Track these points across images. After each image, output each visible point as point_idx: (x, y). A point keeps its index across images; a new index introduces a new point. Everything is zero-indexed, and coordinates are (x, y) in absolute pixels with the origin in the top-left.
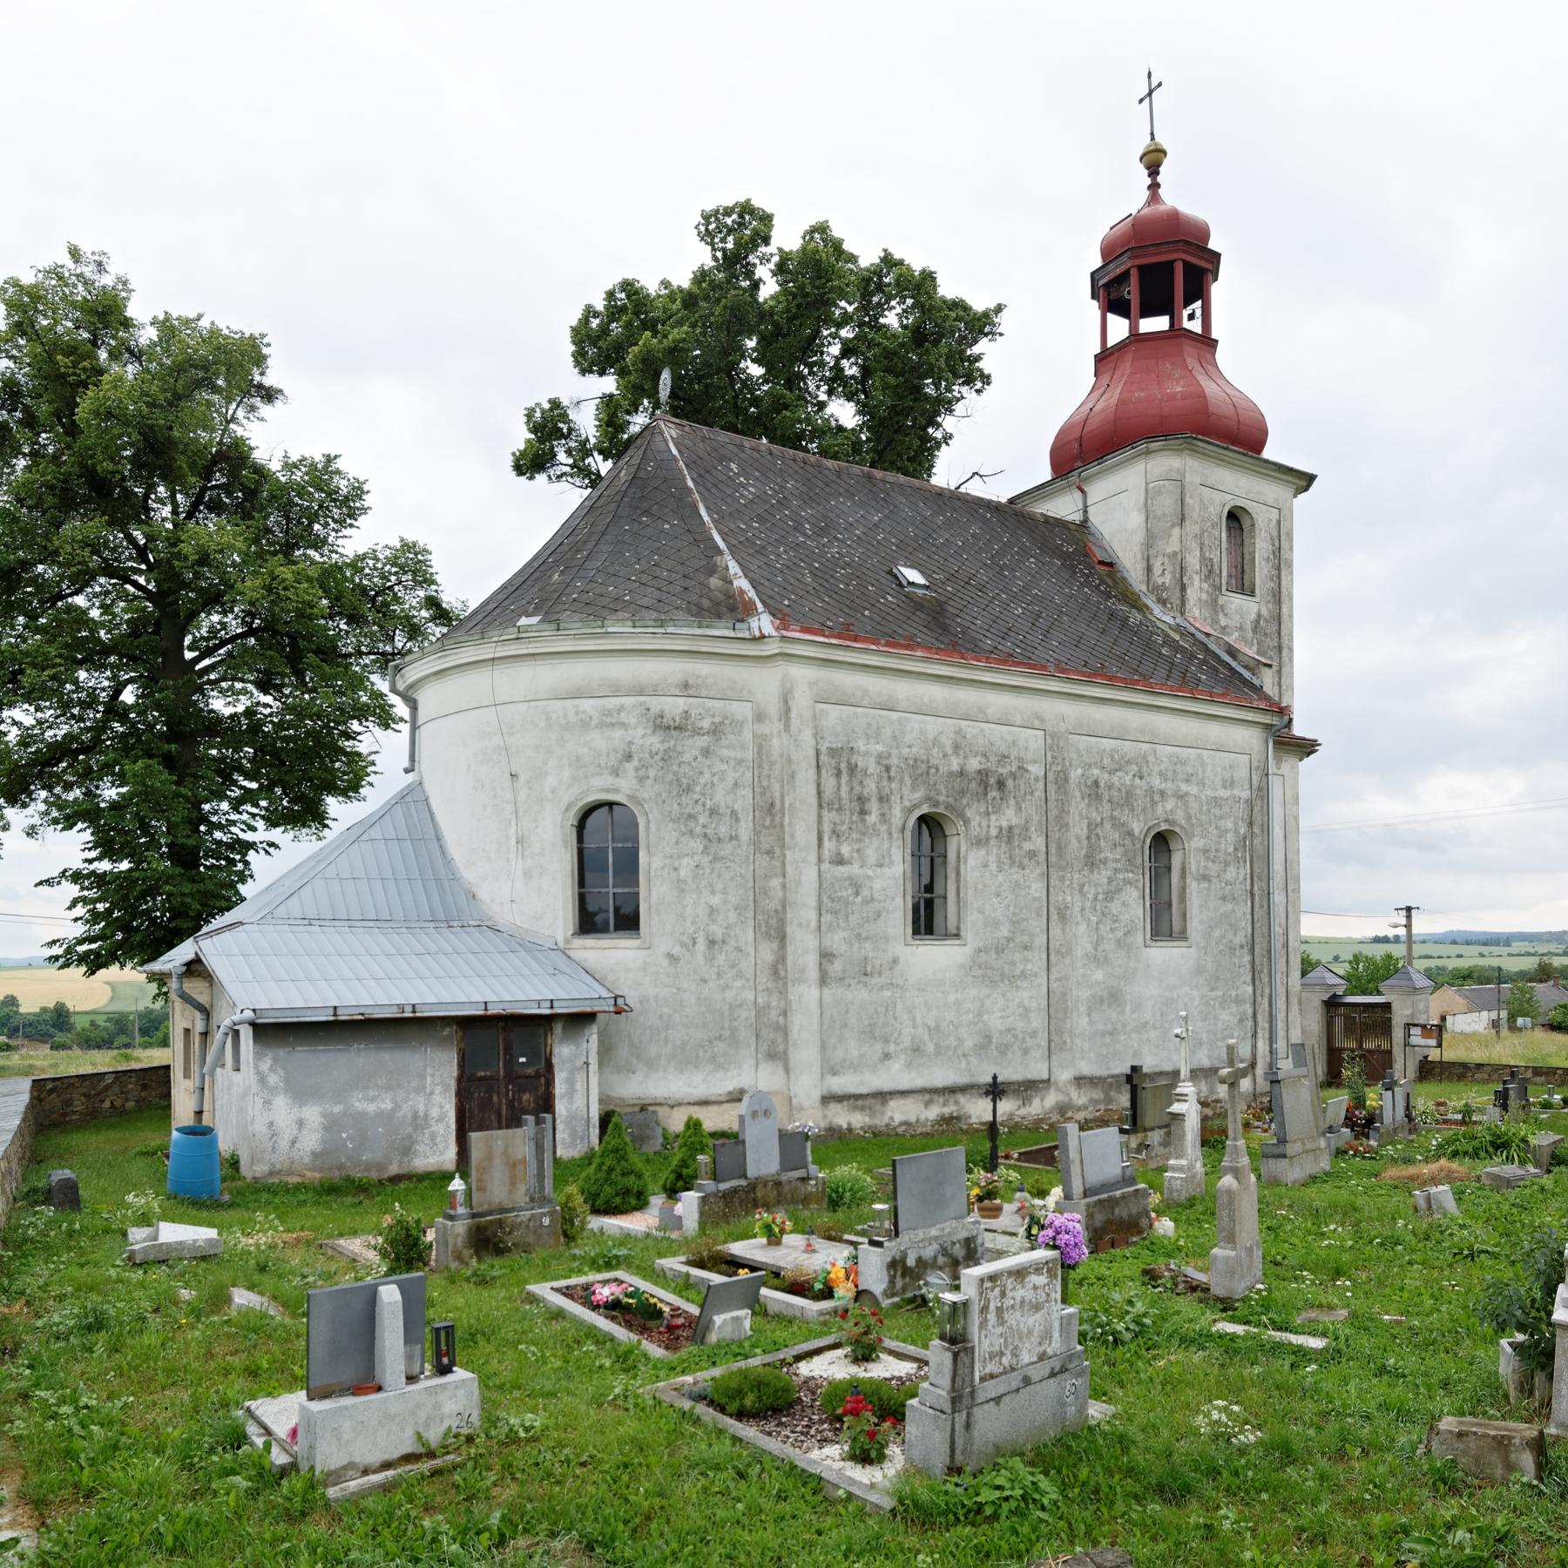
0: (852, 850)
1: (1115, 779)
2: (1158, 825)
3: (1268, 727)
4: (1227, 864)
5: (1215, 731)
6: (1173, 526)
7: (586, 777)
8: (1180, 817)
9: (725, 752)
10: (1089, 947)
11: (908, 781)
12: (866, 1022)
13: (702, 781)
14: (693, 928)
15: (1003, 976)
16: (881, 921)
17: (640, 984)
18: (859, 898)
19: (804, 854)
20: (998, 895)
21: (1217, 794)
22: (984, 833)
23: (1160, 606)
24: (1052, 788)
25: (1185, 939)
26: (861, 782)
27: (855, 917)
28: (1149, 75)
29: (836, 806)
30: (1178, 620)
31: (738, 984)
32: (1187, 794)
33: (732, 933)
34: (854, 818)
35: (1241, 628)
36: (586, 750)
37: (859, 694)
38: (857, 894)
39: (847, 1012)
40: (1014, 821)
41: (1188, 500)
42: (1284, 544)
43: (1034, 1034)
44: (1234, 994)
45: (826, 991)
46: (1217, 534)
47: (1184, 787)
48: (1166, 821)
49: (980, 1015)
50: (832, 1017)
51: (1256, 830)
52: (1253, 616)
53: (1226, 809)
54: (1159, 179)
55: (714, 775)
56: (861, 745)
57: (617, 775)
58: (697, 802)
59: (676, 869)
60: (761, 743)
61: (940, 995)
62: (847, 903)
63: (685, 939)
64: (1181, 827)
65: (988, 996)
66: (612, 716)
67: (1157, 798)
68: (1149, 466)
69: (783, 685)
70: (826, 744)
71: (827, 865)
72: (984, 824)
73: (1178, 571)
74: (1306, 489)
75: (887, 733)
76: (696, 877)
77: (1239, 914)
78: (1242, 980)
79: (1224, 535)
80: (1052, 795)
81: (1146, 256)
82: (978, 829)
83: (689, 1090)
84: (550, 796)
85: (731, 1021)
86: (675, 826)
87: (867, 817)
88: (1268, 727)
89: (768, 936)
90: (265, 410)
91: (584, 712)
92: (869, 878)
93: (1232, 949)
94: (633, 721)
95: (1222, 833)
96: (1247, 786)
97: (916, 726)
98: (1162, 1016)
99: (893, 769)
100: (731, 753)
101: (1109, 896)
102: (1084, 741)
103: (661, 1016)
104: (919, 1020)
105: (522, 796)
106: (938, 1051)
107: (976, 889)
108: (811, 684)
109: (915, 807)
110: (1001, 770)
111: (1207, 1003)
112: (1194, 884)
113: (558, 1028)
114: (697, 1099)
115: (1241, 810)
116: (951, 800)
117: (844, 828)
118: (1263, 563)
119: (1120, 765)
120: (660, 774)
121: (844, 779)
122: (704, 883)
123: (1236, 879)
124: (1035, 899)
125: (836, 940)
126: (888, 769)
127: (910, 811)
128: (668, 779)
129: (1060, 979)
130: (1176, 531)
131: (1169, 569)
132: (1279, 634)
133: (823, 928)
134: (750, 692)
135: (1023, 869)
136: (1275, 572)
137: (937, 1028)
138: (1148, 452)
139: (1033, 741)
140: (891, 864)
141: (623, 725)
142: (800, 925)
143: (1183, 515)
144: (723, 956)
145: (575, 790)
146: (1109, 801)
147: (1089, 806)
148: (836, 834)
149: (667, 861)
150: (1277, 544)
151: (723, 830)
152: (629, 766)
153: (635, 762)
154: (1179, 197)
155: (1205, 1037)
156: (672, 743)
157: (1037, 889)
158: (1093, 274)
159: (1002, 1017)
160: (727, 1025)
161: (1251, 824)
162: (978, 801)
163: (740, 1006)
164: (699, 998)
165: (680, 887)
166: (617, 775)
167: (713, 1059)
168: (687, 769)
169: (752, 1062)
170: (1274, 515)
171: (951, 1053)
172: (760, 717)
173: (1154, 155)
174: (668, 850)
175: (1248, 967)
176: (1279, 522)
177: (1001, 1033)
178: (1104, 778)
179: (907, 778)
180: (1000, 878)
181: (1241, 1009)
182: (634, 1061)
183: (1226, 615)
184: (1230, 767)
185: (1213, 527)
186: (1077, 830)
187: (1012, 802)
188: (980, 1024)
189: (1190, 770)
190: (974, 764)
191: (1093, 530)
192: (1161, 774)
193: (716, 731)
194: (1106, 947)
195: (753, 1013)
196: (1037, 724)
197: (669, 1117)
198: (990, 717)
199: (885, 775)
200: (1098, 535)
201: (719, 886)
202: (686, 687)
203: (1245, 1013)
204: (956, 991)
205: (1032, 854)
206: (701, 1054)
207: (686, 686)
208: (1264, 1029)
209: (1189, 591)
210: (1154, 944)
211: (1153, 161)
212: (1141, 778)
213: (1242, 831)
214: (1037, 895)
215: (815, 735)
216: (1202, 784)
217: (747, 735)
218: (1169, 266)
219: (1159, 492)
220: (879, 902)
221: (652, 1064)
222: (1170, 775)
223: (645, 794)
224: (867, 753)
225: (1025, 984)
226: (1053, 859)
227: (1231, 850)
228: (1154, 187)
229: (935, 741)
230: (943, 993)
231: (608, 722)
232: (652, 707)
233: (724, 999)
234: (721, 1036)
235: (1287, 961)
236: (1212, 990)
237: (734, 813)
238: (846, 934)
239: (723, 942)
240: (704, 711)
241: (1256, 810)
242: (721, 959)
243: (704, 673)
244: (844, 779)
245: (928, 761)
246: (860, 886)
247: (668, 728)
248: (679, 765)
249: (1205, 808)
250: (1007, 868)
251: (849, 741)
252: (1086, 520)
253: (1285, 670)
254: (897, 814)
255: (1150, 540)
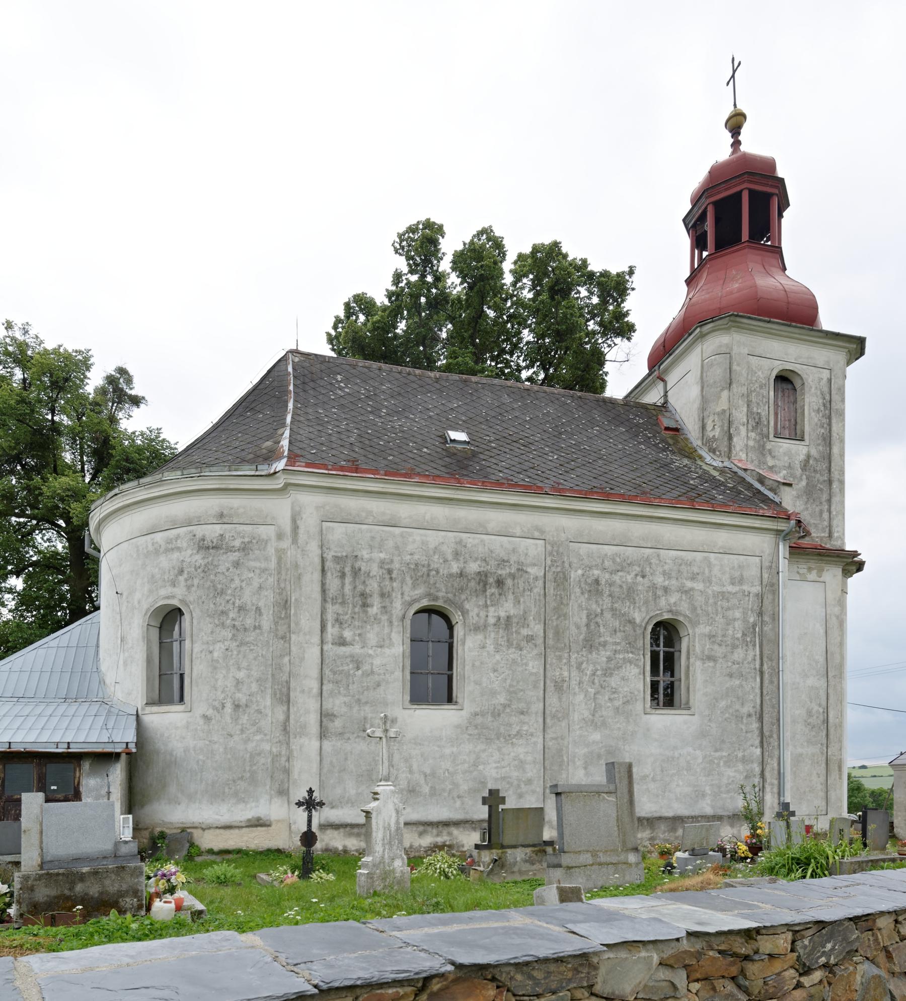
0: (354, 635)
1: (616, 578)
2: (661, 614)
3: (778, 532)
4: (734, 647)
5: (722, 538)
6: (722, 390)
7: (157, 589)
8: (684, 608)
9: (252, 564)
10: (586, 714)
11: (409, 581)
12: (364, 768)
13: (233, 586)
14: (223, 696)
15: (498, 736)
16: (381, 690)
17: (184, 738)
18: (360, 672)
19: (308, 637)
20: (495, 671)
21: (724, 589)
22: (482, 621)
23: (711, 454)
24: (550, 586)
25: (689, 708)
26: (364, 582)
27: (355, 686)
29: (340, 601)
30: (727, 464)
31: (258, 737)
32: (692, 589)
33: (254, 699)
34: (357, 610)
35: (790, 467)
36: (157, 570)
37: (364, 514)
38: (358, 668)
39: (346, 759)
40: (512, 612)
41: (735, 367)
42: (835, 397)
43: (529, 782)
44: (740, 755)
45: (327, 745)
46: (765, 393)
47: (689, 584)
48: (670, 611)
49: (475, 765)
50: (331, 762)
51: (766, 618)
52: (802, 457)
53: (734, 601)
54: (740, 138)
55: (243, 581)
56: (365, 554)
57: (174, 586)
58: (228, 601)
59: (211, 652)
60: (280, 554)
61: (437, 749)
62: (348, 675)
63: (216, 703)
64: (685, 616)
65: (484, 750)
66: (172, 543)
67: (659, 593)
68: (705, 347)
69: (292, 508)
70: (332, 553)
71: (330, 646)
72: (483, 614)
73: (726, 424)
74: (862, 353)
75: (390, 543)
76: (225, 657)
77: (747, 688)
78: (749, 743)
79: (772, 393)
80: (551, 591)
81: (719, 193)
82: (476, 618)
83: (217, 817)
84: (137, 606)
85: (251, 766)
86: (211, 620)
87: (369, 609)
88: (778, 532)
89: (281, 701)
90: (135, 411)
91: (157, 543)
92: (370, 656)
93: (739, 718)
94: (185, 545)
95: (729, 622)
96: (757, 582)
97: (418, 538)
98: (662, 771)
99: (395, 572)
100: (257, 564)
101: (608, 672)
102: (584, 549)
103: (198, 762)
104: (415, 767)
105: (124, 609)
106: (433, 792)
107: (473, 665)
108: (317, 508)
109: (414, 601)
110: (500, 572)
111: (711, 762)
112: (698, 663)
113: (86, 765)
114: (223, 824)
115: (751, 603)
116: (450, 596)
117: (346, 617)
118: (813, 414)
119: (623, 566)
120: (201, 582)
121: (348, 580)
122: (231, 662)
123: (745, 659)
124: (531, 674)
125: (336, 704)
126: (390, 572)
127: (410, 604)
128: (206, 586)
129: (553, 739)
130: (725, 394)
131: (718, 424)
132: (830, 471)
133: (324, 693)
134: (273, 518)
135: (521, 650)
136: (825, 421)
137: (433, 774)
138: (702, 336)
139: (534, 549)
140: (391, 645)
141: (179, 549)
142: (303, 691)
143: (731, 380)
144: (246, 717)
145: (151, 600)
146: (610, 595)
147: (589, 599)
148: (338, 621)
149: (204, 647)
150: (828, 398)
151: (249, 622)
152: (181, 578)
153: (185, 575)
154: (752, 144)
155: (708, 790)
156: (210, 559)
157: (534, 666)
158: (684, 220)
159: (497, 768)
160: (248, 768)
161: (761, 614)
162: (477, 596)
163: (259, 754)
164: (226, 748)
165: (214, 666)
166: (174, 586)
167: (236, 794)
168: (221, 577)
169: (267, 797)
170: (825, 374)
171: (446, 794)
172: (280, 536)
173: (739, 118)
174: (205, 638)
175: (757, 732)
176: (830, 380)
177: (496, 780)
178: (605, 577)
179: (408, 579)
180: (498, 657)
181: (748, 767)
182: (180, 795)
183: (774, 457)
184: (739, 567)
185: (761, 387)
186: (576, 619)
187: (511, 597)
188: (475, 773)
189: (696, 570)
190: (473, 567)
191: (671, 408)
192: (664, 573)
193: (245, 549)
194: (604, 713)
195: (269, 760)
196: (536, 534)
197: (202, 837)
198: (490, 530)
199: (387, 576)
200: (674, 412)
201: (245, 664)
202: (221, 517)
203: (752, 770)
204: (452, 746)
205: (530, 639)
206: (227, 790)
207: (222, 515)
208: (772, 784)
209: (735, 439)
210: (654, 711)
211: (735, 124)
212: (643, 577)
213: (752, 620)
214: (534, 671)
215: (322, 547)
216: (708, 581)
217: (271, 551)
218: (739, 195)
219: (712, 365)
220: (379, 675)
221: (191, 798)
222: (674, 574)
223: (191, 598)
224: (370, 560)
225: (521, 741)
226: (550, 642)
227: (739, 635)
229: (436, 550)
230: (439, 746)
231: (171, 548)
232: (197, 533)
233: (246, 749)
234: (242, 777)
235: (827, 735)
236: (716, 751)
237: (258, 610)
238: (346, 699)
239: (247, 706)
240: (235, 534)
241: (766, 602)
242: (244, 719)
243: (236, 506)
244: (348, 580)
245: (429, 565)
246: (361, 662)
247: (208, 548)
248: (216, 575)
249: (711, 601)
250: (504, 649)
251: (353, 551)
252: (666, 402)
253: (835, 500)
254: (397, 607)
255: (705, 402)
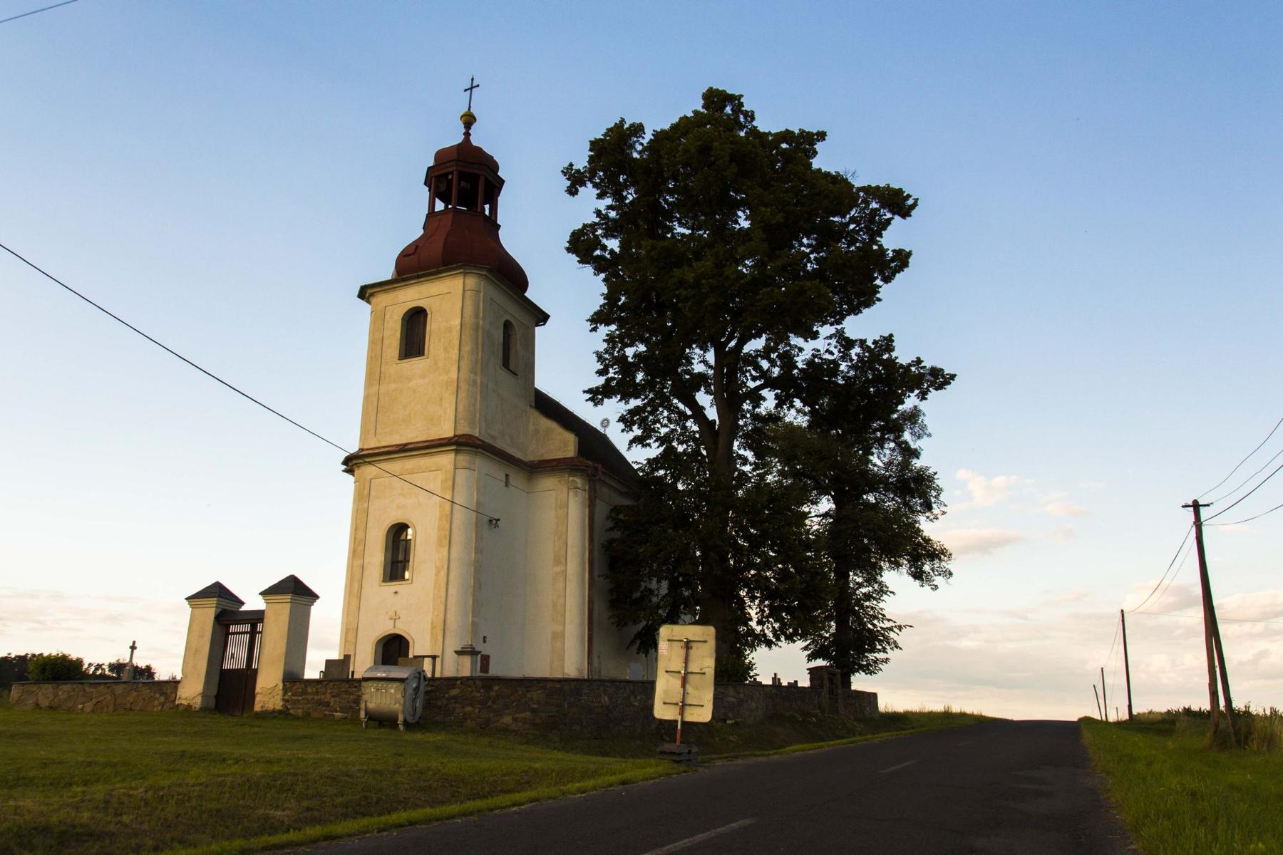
28: (473, 79)
211: (469, 120)
228: (467, 134)
